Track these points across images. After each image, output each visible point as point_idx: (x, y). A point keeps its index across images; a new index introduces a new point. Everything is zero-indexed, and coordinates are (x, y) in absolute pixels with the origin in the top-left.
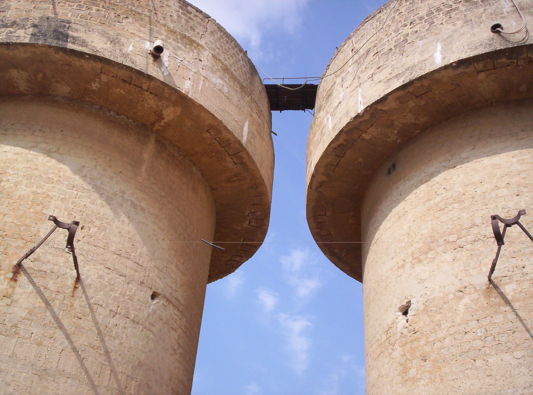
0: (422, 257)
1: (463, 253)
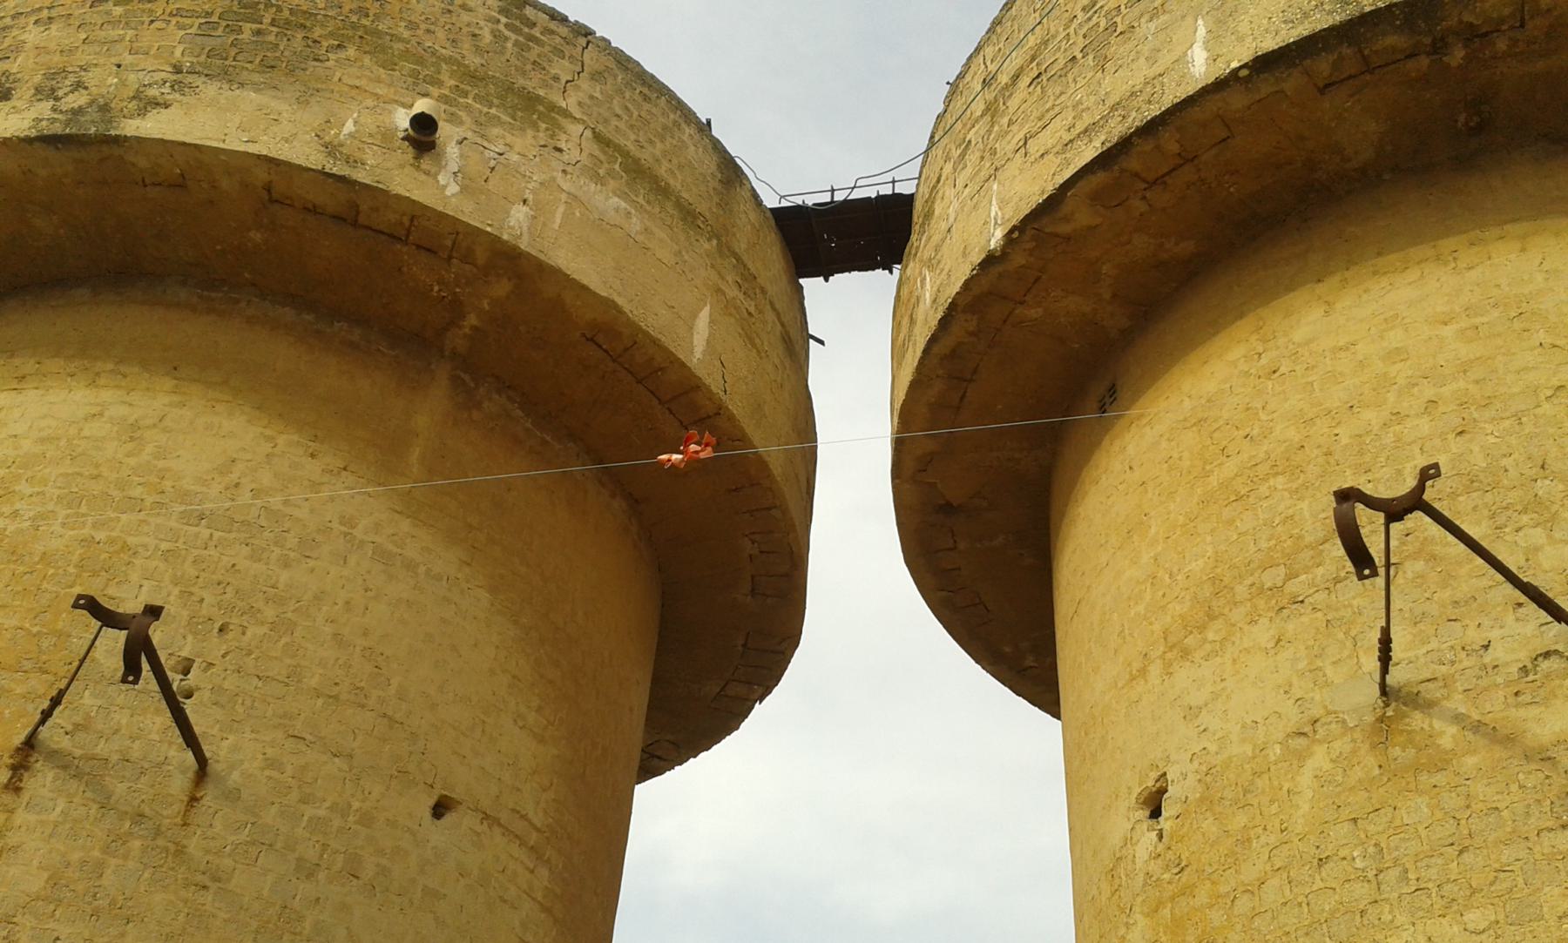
0: (1190, 641)
1: (1304, 619)
